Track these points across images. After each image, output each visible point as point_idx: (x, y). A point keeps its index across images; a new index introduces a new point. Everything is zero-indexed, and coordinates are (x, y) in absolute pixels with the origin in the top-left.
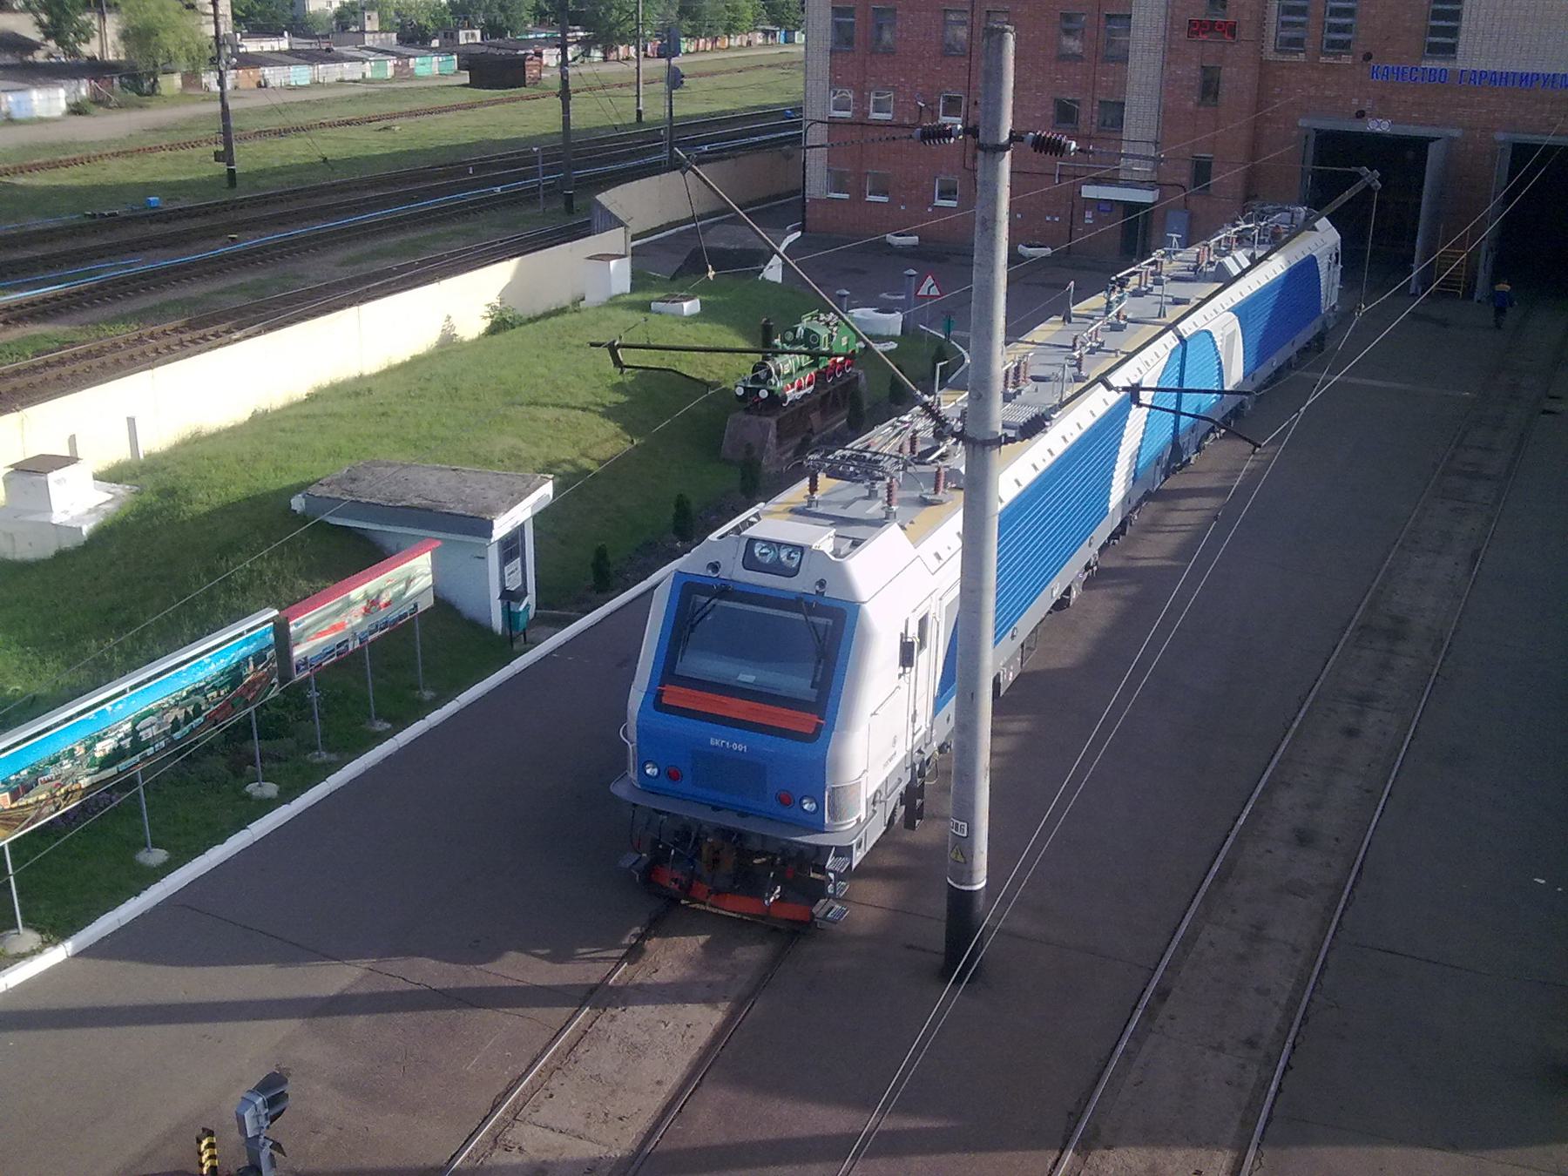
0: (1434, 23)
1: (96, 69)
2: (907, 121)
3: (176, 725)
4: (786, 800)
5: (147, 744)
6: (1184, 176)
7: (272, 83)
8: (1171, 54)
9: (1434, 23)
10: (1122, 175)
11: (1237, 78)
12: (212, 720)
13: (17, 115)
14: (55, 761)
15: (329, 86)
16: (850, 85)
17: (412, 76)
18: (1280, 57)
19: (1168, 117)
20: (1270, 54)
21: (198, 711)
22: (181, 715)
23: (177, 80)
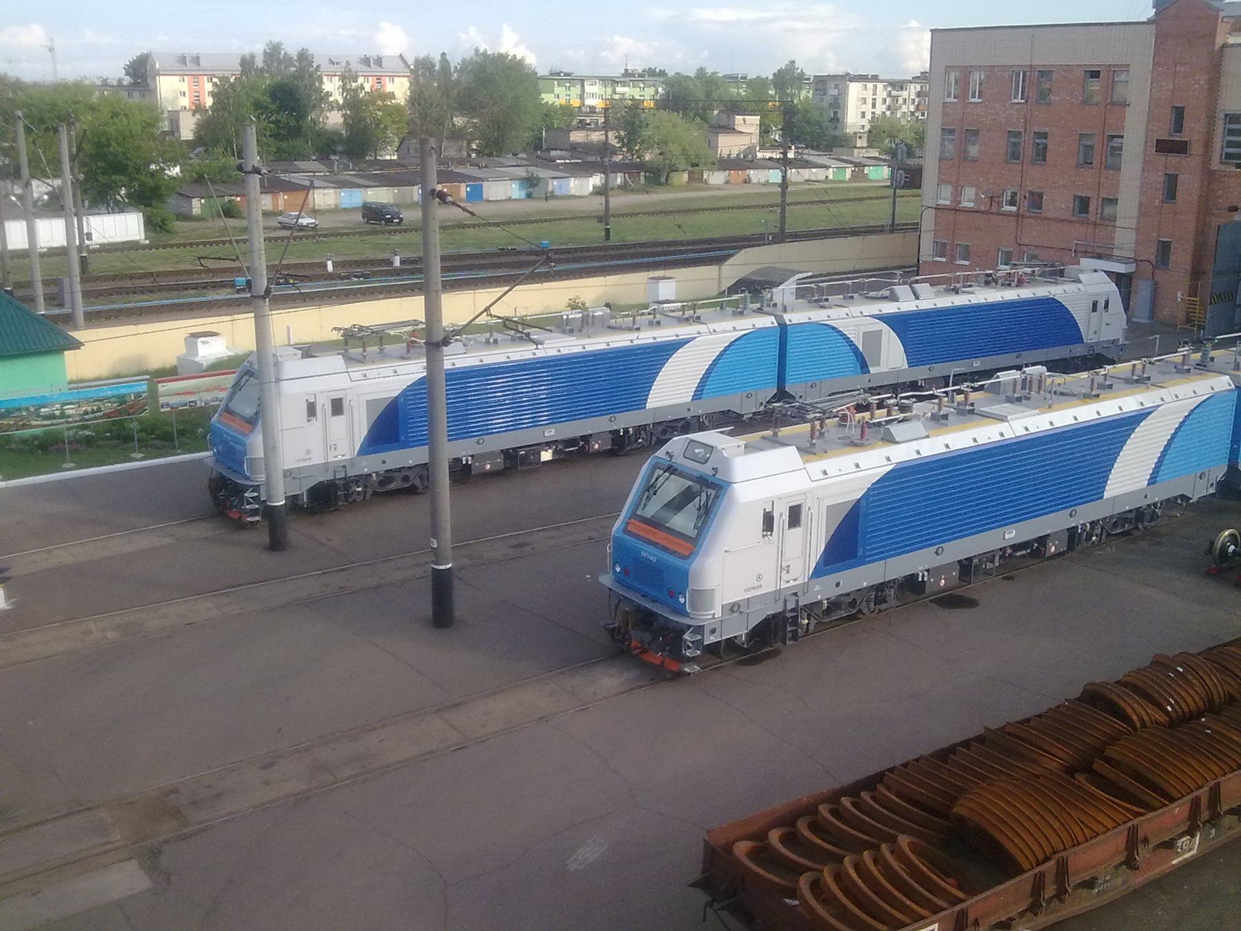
0: (1230, 138)
1: (641, 166)
2: (982, 208)
3: (86, 413)
4: (672, 595)
5: (69, 416)
6: (1151, 253)
7: (754, 180)
8: (1147, 166)
9: (1230, 138)
10: (1116, 252)
11: (1190, 186)
12: (108, 416)
13: (557, 193)
14: (19, 409)
15: (801, 183)
16: (950, 182)
17: (865, 177)
18: (1223, 168)
19: (1143, 211)
20: (1215, 165)
21: (99, 410)
22: (89, 409)
23: (686, 176)
